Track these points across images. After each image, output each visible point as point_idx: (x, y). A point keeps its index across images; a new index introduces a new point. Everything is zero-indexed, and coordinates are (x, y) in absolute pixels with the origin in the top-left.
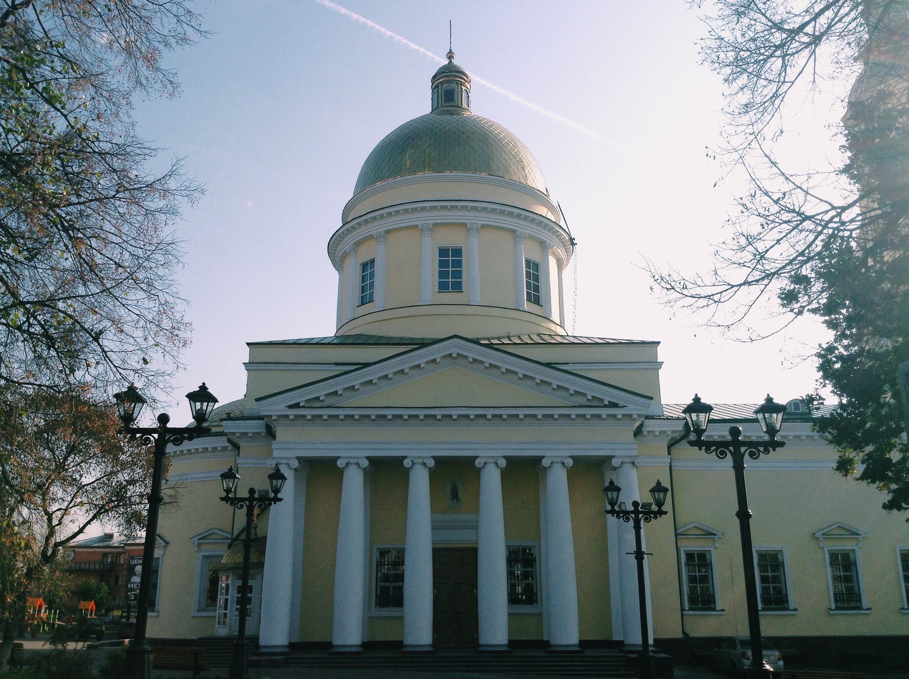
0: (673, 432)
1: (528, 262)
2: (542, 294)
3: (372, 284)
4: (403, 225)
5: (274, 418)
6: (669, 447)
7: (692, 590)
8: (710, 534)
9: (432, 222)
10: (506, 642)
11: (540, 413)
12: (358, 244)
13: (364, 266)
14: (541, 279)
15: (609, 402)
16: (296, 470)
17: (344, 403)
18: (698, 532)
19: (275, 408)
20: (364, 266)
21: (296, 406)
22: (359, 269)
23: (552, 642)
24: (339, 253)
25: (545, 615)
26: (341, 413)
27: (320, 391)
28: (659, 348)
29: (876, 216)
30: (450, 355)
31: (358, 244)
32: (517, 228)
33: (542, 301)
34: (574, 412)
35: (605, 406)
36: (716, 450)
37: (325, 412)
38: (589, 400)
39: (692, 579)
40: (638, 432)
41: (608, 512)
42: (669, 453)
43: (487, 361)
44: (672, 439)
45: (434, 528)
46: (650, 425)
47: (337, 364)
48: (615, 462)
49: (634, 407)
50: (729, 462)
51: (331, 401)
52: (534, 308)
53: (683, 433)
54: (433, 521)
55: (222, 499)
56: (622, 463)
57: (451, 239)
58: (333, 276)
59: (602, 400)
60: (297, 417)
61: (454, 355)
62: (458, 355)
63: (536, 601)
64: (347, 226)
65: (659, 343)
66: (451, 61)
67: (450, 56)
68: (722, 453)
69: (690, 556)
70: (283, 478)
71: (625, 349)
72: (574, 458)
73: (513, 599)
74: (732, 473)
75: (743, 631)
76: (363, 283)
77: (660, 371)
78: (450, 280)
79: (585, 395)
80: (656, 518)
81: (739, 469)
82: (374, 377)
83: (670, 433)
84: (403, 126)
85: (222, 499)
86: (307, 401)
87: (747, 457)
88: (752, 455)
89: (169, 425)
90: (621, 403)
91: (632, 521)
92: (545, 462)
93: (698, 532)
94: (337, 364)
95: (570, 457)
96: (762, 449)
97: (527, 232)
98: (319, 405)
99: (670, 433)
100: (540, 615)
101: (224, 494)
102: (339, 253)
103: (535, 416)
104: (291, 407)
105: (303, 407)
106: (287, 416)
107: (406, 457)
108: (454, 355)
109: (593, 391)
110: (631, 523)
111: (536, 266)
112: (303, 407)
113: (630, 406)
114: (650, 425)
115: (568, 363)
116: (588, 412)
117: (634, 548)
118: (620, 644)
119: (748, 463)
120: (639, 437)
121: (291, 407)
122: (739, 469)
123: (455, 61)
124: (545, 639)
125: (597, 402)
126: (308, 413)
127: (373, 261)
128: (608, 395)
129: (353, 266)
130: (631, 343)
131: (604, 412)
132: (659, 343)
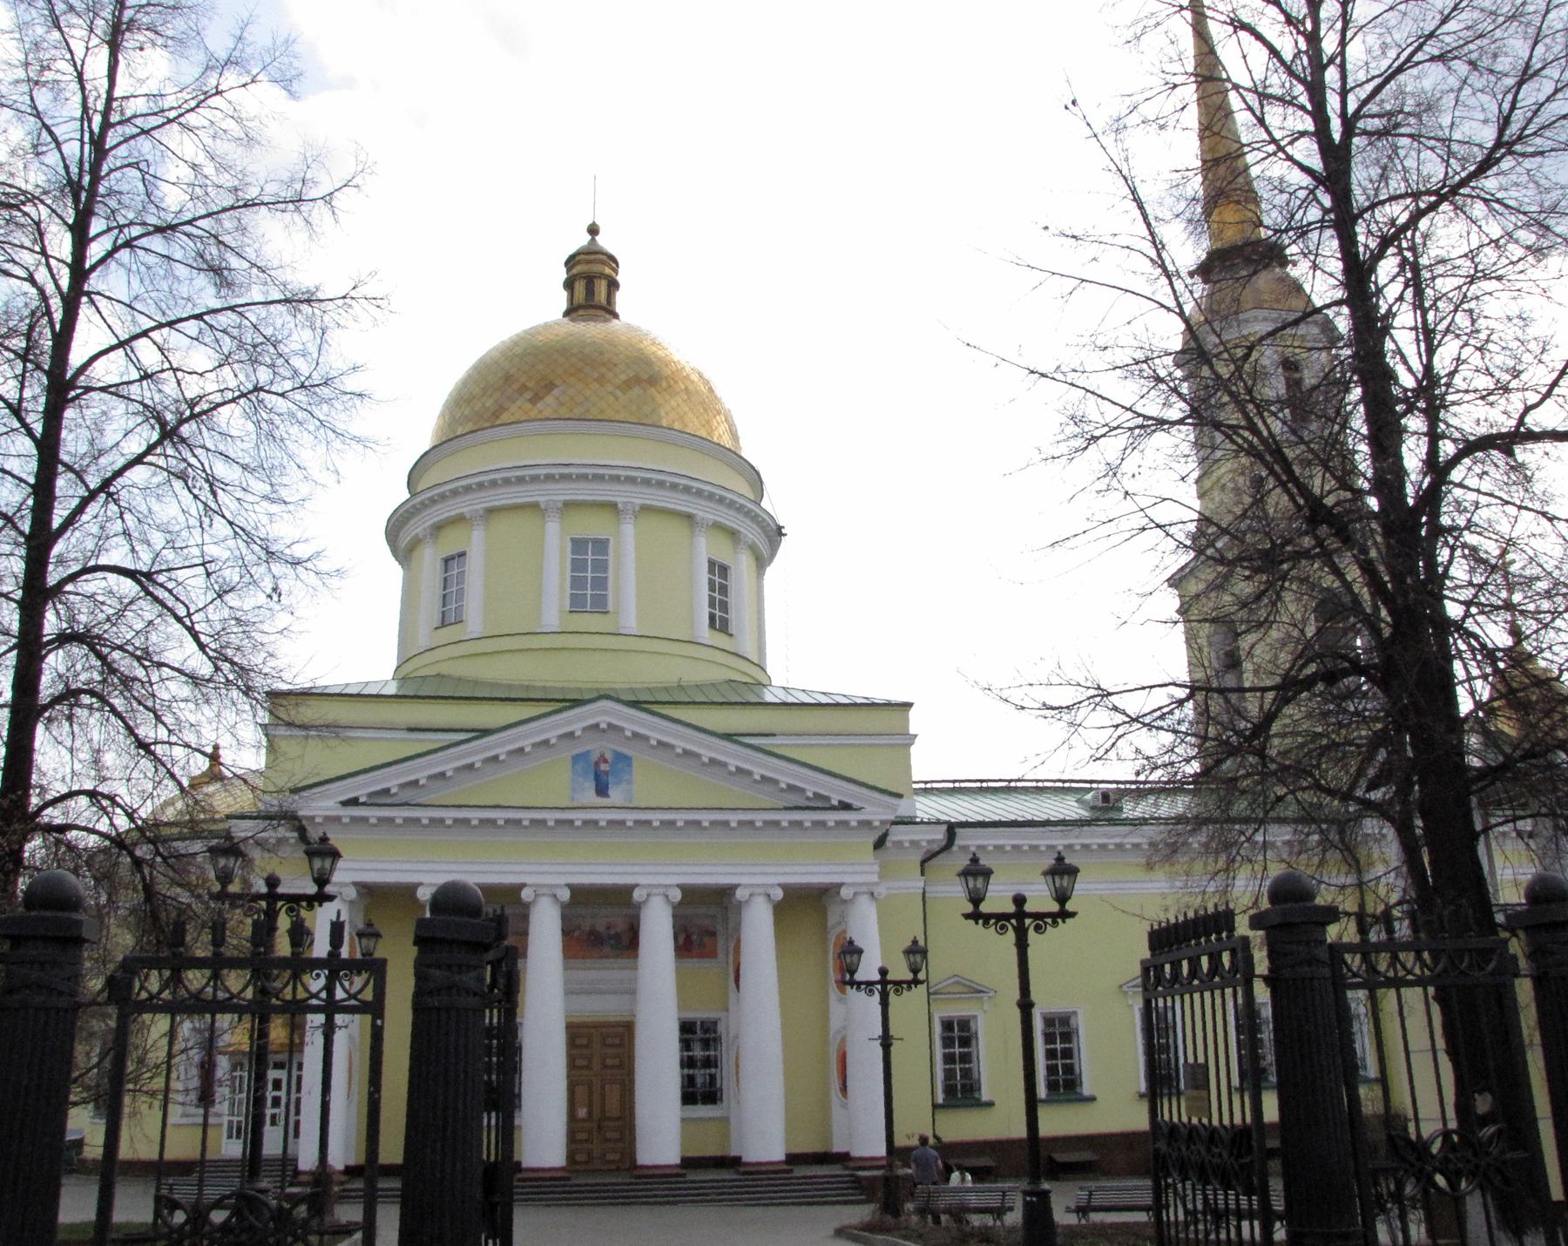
0: (929, 842)
1: (712, 564)
2: (732, 616)
3: (461, 592)
4: (519, 501)
5: (318, 820)
6: (923, 862)
7: (949, 1075)
8: (977, 991)
9: (562, 498)
10: (678, 1161)
11: (733, 818)
12: (438, 528)
13: (447, 561)
14: (732, 592)
15: (840, 802)
16: (351, 902)
17: (432, 796)
18: (960, 989)
19: (320, 804)
20: (447, 561)
21: (354, 802)
22: (439, 565)
23: (745, 1159)
24: (405, 539)
25: (733, 1121)
26: (424, 814)
27: (391, 780)
28: (912, 713)
29: (1261, 433)
30: (597, 725)
31: (438, 528)
32: (694, 512)
33: (733, 629)
34: (785, 818)
35: (833, 808)
36: (996, 924)
37: (399, 814)
38: (808, 798)
39: (949, 1059)
40: (880, 844)
41: (845, 983)
42: (923, 874)
43: (706, 754)
44: (928, 851)
45: (568, 992)
46: (899, 834)
47: (411, 730)
48: (845, 893)
49: (876, 811)
50: (1011, 935)
51: (406, 795)
52: (720, 640)
53: (944, 843)
54: (567, 982)
55: (967, 916)
56: (649, 895)
57: (592, 526)
58: (394, 572)
59: (827, 799)
60: (354, 819)
61: (603, 726)
62: (610, 726)
63: (721, 1100)
64: (418, 500)
65: (908, 705)
66: (593, 239)
67: (593, 230)
68: (1003, 927)
69: (947, 1025)
70: (860, 952)
71: (864, 713)
72: (785, 887)
73: (689, 1098)
74: (1014, 950)
75: (1020, 1131)
76: (444, 589)
77: (913, 748)
78: (589, 592)
79: (802, 790)
80: (1055, 924)
81: (1022, 945)
82: (477, 759)
83: (924, 844)
84: (515, 343)
85: (967, 916)
86: (371, 795)
87: (1031, 933)
88: (1038, 929)
89: (280, 890)
90: (856, 804)
91: (877, 993)
92: (740, 894)
93: (960, 989)
94: (411, 730)
95: (779, 885)
96: (1049, 920)
97: (711, 517)
98: (389, 801)
99: (924, 844)
100: (725, 1120)
101: (969, 908)
102: (405, 539)
103: (726, 824)
104: (345, 803)
105: (364, 804)
106: (338, 819)
107: (523, 886)
108: (603, 726)
109: (813, 784)
110: (877, 997)
111: (724, 570)
112: (364, 804)
113: (869, 808)
114: (899, 834)
115: (774, 735)
116: (807, 817)
117: (879, 1032)
118: (843, 1158)
119: (892, 997)
120: (880, 851)
121: (345, 803)
122: (1022, 945)
123: (603, 241)
124: (734, 1153)
125: (821, 803)
126: (373, 813)
127: (462, 555)
128: (837, 792)
129: (430, 558)
130: (872, 705)
131: (831, 817)
132: (908, 705)
